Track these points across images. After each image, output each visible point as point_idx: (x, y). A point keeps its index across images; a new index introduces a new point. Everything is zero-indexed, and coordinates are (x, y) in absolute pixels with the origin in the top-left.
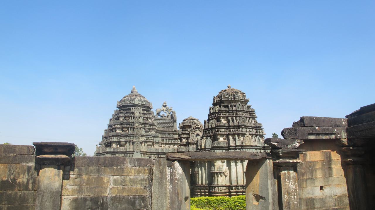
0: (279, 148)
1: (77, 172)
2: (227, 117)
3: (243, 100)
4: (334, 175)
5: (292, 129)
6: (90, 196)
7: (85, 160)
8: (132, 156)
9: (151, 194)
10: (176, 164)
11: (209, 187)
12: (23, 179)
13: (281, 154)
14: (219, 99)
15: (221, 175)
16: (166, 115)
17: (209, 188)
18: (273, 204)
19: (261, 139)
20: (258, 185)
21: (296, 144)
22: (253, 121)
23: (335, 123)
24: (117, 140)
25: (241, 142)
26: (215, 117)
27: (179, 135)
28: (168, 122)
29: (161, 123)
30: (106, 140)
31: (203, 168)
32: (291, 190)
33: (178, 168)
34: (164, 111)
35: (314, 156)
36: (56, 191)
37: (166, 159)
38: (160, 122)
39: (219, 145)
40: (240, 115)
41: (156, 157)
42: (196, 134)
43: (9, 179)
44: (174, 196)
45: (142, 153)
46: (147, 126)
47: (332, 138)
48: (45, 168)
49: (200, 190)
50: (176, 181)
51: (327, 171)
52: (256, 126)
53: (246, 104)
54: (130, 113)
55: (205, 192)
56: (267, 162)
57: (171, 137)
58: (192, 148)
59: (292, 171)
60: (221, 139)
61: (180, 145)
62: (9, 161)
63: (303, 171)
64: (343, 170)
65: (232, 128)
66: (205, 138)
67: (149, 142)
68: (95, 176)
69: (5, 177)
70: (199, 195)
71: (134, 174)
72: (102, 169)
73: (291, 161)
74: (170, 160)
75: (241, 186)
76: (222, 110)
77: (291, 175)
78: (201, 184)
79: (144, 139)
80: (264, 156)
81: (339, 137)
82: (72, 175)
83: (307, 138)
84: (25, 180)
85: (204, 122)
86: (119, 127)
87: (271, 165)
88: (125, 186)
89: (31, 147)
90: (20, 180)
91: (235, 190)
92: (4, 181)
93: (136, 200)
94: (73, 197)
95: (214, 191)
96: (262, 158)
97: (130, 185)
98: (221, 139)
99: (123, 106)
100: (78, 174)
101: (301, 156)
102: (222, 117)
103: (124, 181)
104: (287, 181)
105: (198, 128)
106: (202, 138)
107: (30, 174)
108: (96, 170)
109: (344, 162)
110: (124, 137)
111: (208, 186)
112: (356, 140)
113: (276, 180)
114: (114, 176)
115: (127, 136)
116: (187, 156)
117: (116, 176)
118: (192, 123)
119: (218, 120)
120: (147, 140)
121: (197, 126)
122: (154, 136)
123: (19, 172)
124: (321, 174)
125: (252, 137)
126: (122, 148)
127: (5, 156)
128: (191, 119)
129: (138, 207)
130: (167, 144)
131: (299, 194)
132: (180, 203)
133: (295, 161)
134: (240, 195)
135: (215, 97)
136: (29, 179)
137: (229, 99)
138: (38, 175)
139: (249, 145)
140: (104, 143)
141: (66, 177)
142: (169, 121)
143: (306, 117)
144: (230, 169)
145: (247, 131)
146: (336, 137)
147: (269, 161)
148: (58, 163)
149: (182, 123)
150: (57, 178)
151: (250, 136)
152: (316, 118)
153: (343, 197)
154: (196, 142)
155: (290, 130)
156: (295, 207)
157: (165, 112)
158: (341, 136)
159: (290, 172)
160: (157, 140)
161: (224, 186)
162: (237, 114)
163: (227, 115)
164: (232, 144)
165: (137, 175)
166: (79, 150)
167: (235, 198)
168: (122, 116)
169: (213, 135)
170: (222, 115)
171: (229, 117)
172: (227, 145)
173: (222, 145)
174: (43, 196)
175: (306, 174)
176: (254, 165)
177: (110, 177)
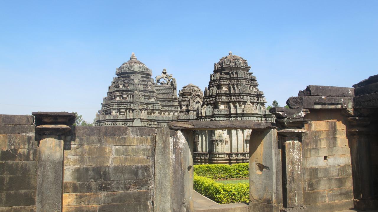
0: (284, 118)
1: (78, 142)
2: (228, 85)
3: (244, 67)
4: (339, 145)
5: (298, 98)
6: (91, 166)
7: (86, 130)
8: (132, 123)
9: (154, 164)
10: (180, 133)
11: (210, 154)
12: (23, 149)
13: (286, 124)
14: (220, 66)
15: (221, 143)
16: (166, 82)
17: (210, 155)
18: (277, 174)
19: (262, 107)
20: (261, 154)
21: (302, 114)
22: (255, 89)
23: (341, 92)
24: (117, 108)
25: (242, 110)
26: (216, 85)
27: (179, 102)
28: (168, 89)
29: (161, 90)
30: (105, 108)
31: (204, 136)
32: (295, 160)
33: (181, 137)
34: (164, 78)
35: (320, 126)
36: (57, 161)
37: (169, 128)
38: (159, 89)
39: (219, 113)
40: (241, 83)
41: (156, 125)
42: (196, 101)
43: (10, 150)
44: (177, 166)
45: (142, 120)
46: (147, 93)
47: (338, 108)
48: (46, 139)
49: (201, 158)
50: (179, 151)
51: (331, 141)
52: (257, 94)
53: (248, 71)
54: (129, 80)
55: (205, 160)
56: (271, 132)
57: (172, 104)
58: (192, 115)
59: (296, 140)
60: (222, 107)
61: (180, 112)
62: (8, 131)
63: (307, 141)
64: (347, 140)
65: (233, 96)
66: (205, 105)
67: (149, 109)
68: (97, 146)
69: (5, 147)
70: (199, 162)
71: (136, 143)
72: (103, 139)
73: (296, 131)
74: (174, 130)
75: (241, 154)
76: (223, 78)
77: (296, 145)
78: (201, 151)
79: (145, 106)
80: (269, 126)
81: (345, 107)
82: (73, 145)
83: (312, 108)
84: (26, 151)
85: (205, 90)
86: (118, 94)
87: (275, 134)
88: (127, 156)
89: (30, 117)
90: (20, 151)
91: (235, 158)
92: (5, 151)
93: (139, 170)
94: (74, 167)
95: (214, 158)
96: (267, 127)
97: (132, 155)
98: (222, 107)
99: (122, 73)
100: (79, 144)
101: (306, 125)
102: (222, 84)
103: (126, 151)
104: (291, 150)
105: (199, 95)
106: (203, 105)
107: (30, 145)
108: (97, 140)
109: (350, 132)
110: (124, 104)
111: (208, 153)
112: (363, 110)
113: (280, 150)
114: (115, 145)
115: (127, 103)
116: (190, 125)
117: (117, 145)
118: (192, 90)
119: (219, 87)
120: (147, 107)
121: (197, 93)
122: (154, 104)
123: (19, 143)
124: (326, 144)
125: (253, 104)
126: (122, 115)
127: (4, 126)
128: (191, 86)
129: (141, 177)
130: (167, 111)
131: (303, 164)
132: (183, 173)
133: (300, 131)
134: (240, 162)
135: (216, 63)
136: (29, 149)
137: (230, 66)
138: (38, 146)
139: (249, 113)
140: (104, 111)
141: (67, 147)
142: (169, 88)
143: (313, 86)
144: (230, 137)
145: (248, 99)
146: (342, 107)
147: (273, 131)
148: (58, 133)
149: (182, 90)
150: (58, 148)
151: (251, 104)
152: (322, 87)
153: (346, 167)
154: (196, 110)
155: (295, 99)
156: (298, 176)
157: (165, 79)
158: (347, 106)
159: (295, 141)
160: (157, 107)
161: (224, 154)
162: (238, 82)
163: (228, 82)
164: (233, 111)
165: (140, 145)
166: (78, 117)
167: (236, 166)
168: (121, 83)
169: (214, 103)
170: (223, 83)
171: (230, 84)
172: (228, 113)
173: (222, 113)
174: (44, 167)
175: (311, 144)
176: (257, 135)
177: (112, 147)
